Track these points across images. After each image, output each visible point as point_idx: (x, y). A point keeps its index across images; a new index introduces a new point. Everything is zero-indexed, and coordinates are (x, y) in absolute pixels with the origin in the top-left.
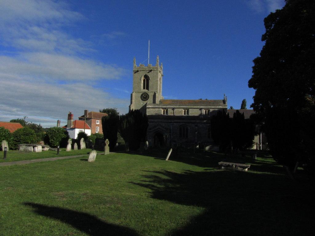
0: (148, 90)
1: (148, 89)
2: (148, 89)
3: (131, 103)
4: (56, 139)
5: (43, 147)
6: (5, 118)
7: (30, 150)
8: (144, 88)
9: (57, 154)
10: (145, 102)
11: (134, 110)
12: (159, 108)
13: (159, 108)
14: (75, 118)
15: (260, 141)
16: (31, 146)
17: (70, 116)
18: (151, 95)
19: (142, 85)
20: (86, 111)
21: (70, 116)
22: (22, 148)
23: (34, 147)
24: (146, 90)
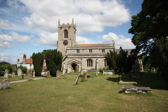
1: (67, 37)
2: (67, 37)
12: (74, 49)
13: (74, 49)
24: (66, 39)
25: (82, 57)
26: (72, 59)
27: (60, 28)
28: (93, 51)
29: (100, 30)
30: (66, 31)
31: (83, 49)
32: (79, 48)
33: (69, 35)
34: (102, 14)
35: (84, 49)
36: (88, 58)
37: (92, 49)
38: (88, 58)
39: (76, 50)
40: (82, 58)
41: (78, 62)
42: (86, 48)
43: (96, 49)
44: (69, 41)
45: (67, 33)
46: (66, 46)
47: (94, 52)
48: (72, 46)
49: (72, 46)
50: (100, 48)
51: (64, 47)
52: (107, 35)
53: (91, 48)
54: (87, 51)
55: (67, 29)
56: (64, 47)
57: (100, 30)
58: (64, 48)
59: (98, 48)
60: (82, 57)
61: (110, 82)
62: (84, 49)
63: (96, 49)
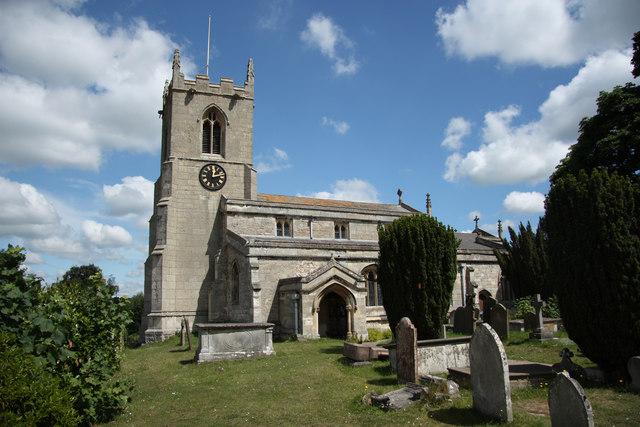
1: (219, 149)
2: (219, 149)
8: (207, 149)
12: (266, 215)
13: (266, 215)
24: (214, 157)
25: (343, 255)
26: (317, 264)
27: (184, 95)
28: (353, 228)
29: (90, 157)
30: (213, 113)
31: (304, 217)
32: (292, 212)
33: (230, 137)
34: (93, 89)
35: (311, 219)
36: (365, 260)
37: (348, 221)
38: (365, 260)
39: (274, 219)
40: (474, 266)
41: (352, 281)
42: (323, 214)
43: (363, 221)
44: (230, 170)
45: (217, 127)
46: (215, 197)
47: (356, 236)
48: (247, 195)
49: (247, 195)
50: (378, 218)
51: (203, 198)
52: (118, 187)
53: (344, 216)
54: (326, 230)
55: (223, 104)
56: (203, 198)
57: (90, 157)
58: (206, 202)
59: (372, 218)
60: (343, 255)
61: (185, 367)
62: (315, 218)
63: (363, 221)
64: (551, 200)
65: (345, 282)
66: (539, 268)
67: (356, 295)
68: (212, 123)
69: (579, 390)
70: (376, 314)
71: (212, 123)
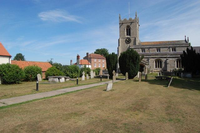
0: (130, 36)
1: (130, 35)
2: (130, 35)
3: (119, 45)
4: (73, 72)
5: (65, 79)
6: (31, 101)
7: (56, 81)
8: (127, 35)
9: (36, 90)
10: (129, 45)
11: (111, 54)
12: (139, 48)
14: (81, 58)
15: (157, 64)
16: (57, 78)
17: (78, 57)
18: (132, 39)
19: (126, 33)
20: (87, 54)
21: (78, 57)
22: (51, 79)
23: (59, 79)
24: (128, 36)
25: (150, 57)
28: (161, 49)
35: (150, 48)
41: (145, 63)
53: (159, 46)
58: (127, 46)
59: (167, 46)
60: (150, 57)
64: (122, 57)
65: (144, 63)
66: (113, 68)
67: (146, 66)
68: (128, 29)
69: (102, 84)
70: (159, 70)
71: (128, 29)
